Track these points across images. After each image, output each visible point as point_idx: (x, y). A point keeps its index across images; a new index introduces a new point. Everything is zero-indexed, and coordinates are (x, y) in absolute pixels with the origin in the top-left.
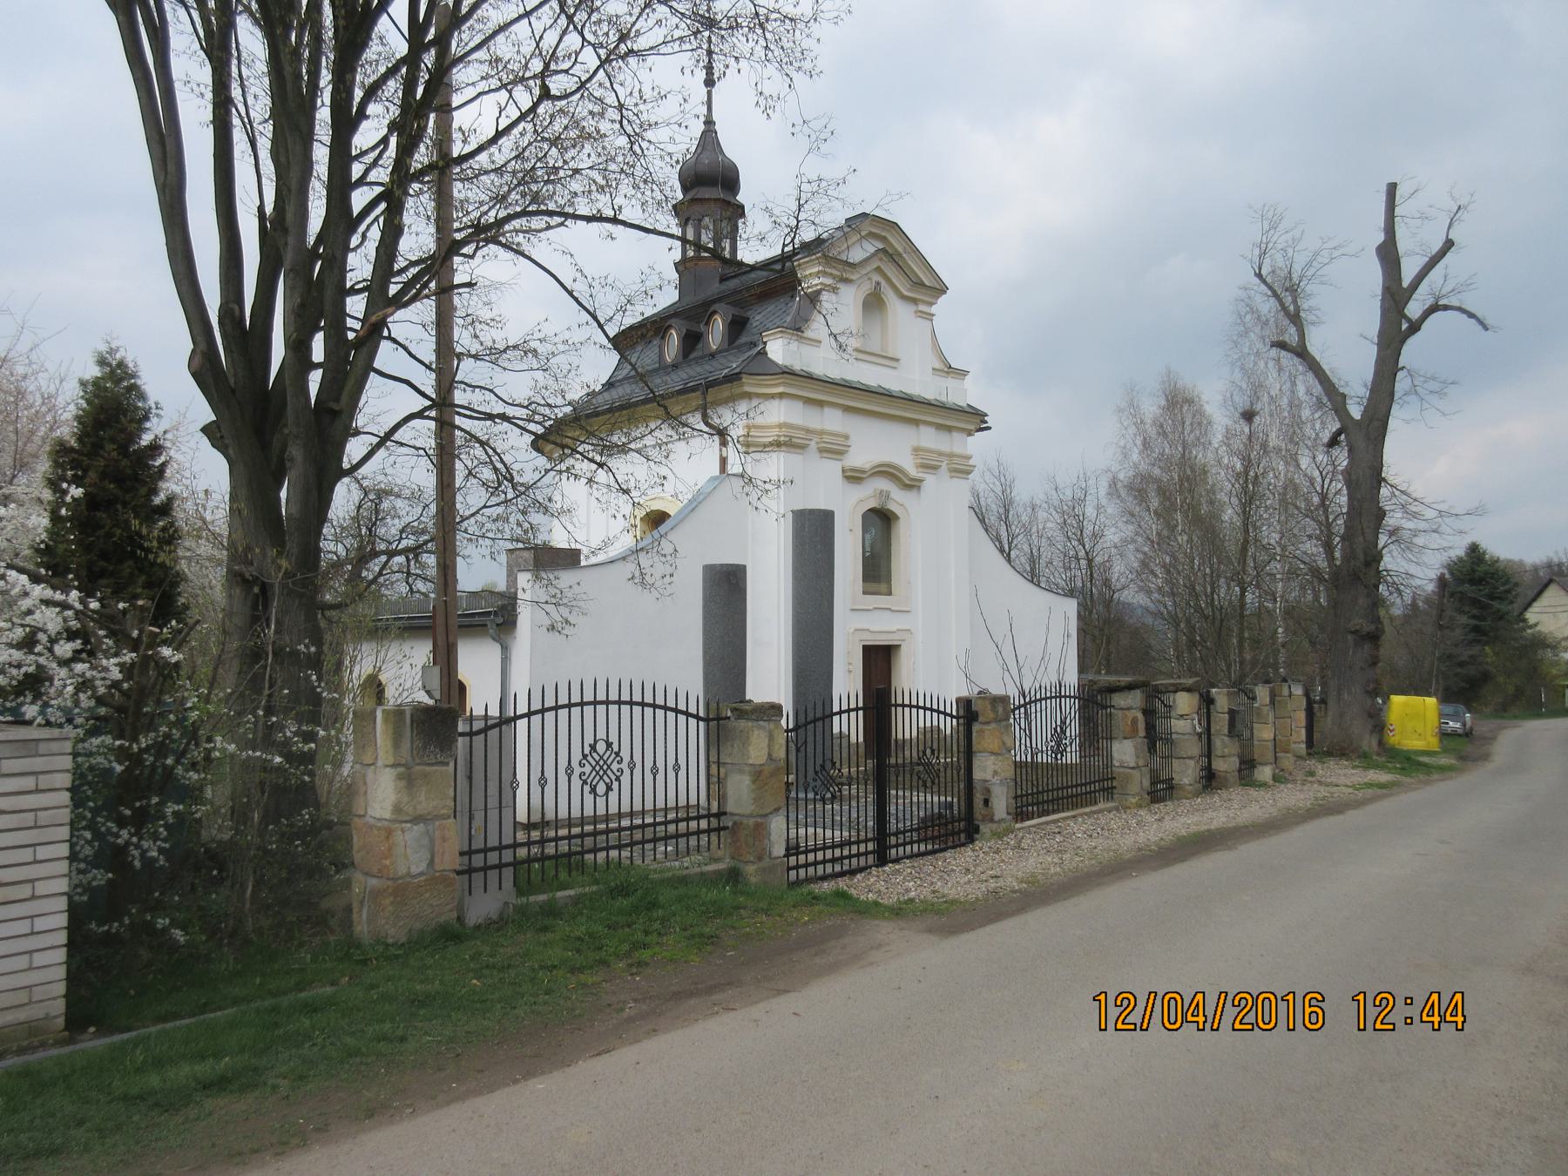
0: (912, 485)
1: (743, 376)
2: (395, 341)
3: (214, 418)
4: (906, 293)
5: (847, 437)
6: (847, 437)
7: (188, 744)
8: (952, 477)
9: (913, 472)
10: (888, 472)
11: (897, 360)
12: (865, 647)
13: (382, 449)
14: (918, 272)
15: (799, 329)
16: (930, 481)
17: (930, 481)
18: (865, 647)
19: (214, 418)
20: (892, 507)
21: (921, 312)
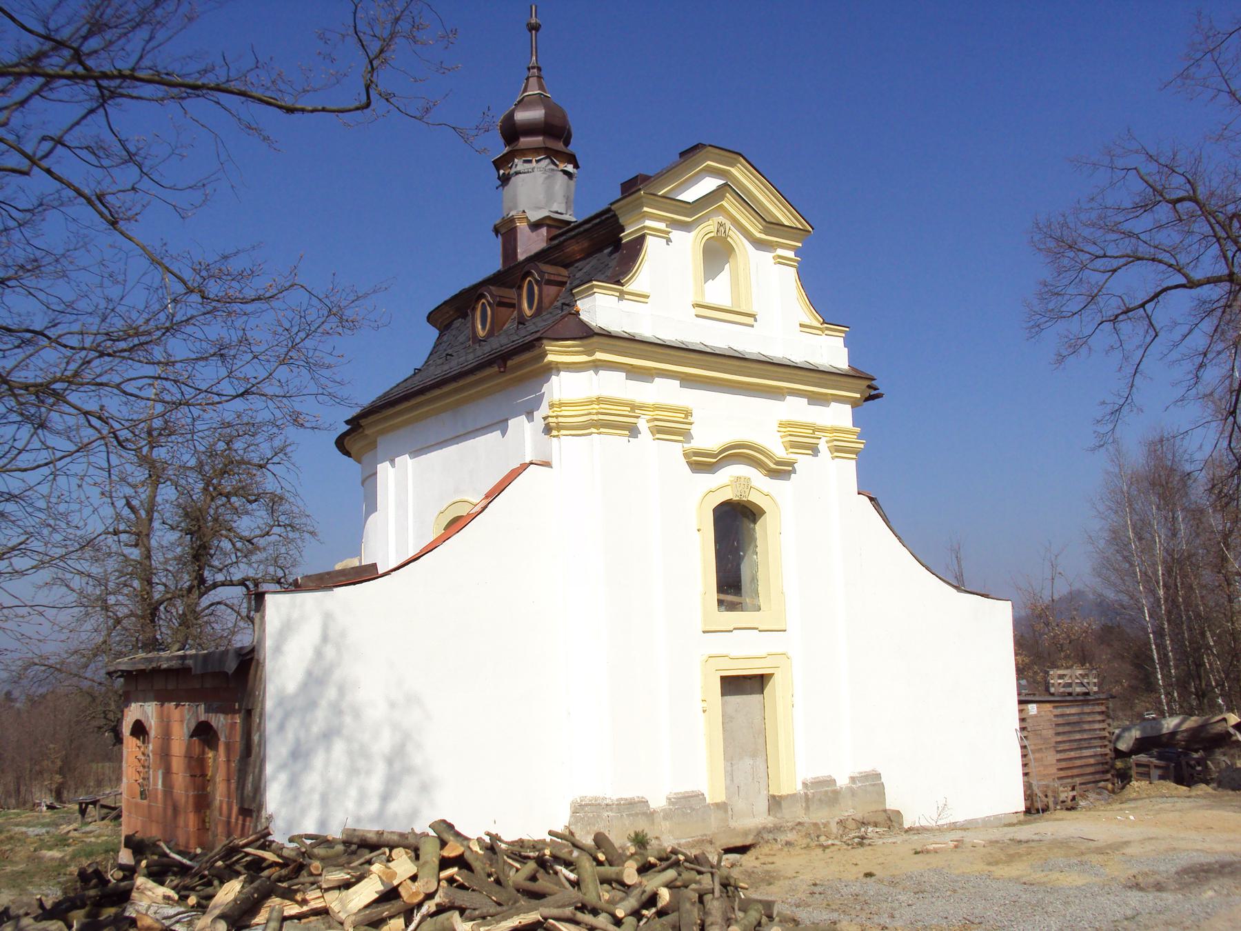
0: (781, 471)
1: (545, 342)
2: (170, 156)
3: (499, 432)
4: (758, 235)
5: (688, 414)
6: (688, 414)
7: (19, 526)
8: (833, 458)
9: (780, 452)
10: (736, 453)
11: (753, 316)
12: (723, 679)
13: (456, 904)
14: (738, 216)
15: (618, 283)
16: (803, 462)
17: (803, 462)
18: (723, 679)
19: (499, 432)
20: (754, 498)
21: (780, 257)
